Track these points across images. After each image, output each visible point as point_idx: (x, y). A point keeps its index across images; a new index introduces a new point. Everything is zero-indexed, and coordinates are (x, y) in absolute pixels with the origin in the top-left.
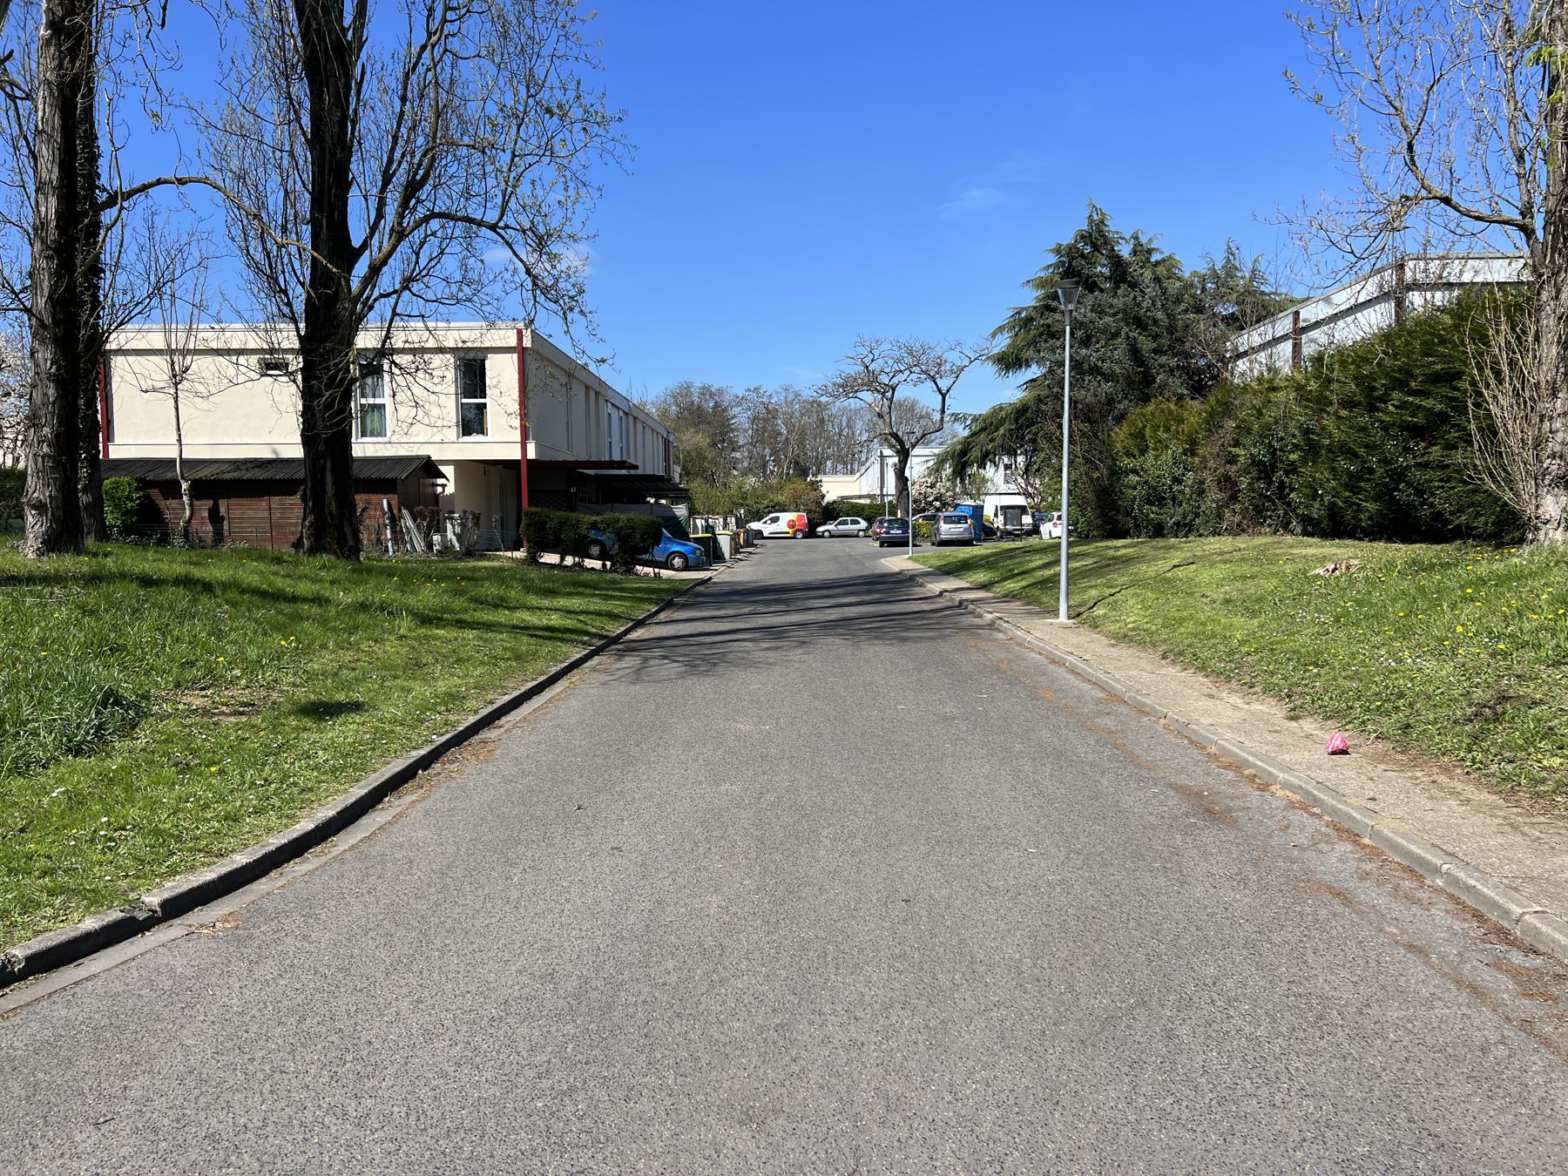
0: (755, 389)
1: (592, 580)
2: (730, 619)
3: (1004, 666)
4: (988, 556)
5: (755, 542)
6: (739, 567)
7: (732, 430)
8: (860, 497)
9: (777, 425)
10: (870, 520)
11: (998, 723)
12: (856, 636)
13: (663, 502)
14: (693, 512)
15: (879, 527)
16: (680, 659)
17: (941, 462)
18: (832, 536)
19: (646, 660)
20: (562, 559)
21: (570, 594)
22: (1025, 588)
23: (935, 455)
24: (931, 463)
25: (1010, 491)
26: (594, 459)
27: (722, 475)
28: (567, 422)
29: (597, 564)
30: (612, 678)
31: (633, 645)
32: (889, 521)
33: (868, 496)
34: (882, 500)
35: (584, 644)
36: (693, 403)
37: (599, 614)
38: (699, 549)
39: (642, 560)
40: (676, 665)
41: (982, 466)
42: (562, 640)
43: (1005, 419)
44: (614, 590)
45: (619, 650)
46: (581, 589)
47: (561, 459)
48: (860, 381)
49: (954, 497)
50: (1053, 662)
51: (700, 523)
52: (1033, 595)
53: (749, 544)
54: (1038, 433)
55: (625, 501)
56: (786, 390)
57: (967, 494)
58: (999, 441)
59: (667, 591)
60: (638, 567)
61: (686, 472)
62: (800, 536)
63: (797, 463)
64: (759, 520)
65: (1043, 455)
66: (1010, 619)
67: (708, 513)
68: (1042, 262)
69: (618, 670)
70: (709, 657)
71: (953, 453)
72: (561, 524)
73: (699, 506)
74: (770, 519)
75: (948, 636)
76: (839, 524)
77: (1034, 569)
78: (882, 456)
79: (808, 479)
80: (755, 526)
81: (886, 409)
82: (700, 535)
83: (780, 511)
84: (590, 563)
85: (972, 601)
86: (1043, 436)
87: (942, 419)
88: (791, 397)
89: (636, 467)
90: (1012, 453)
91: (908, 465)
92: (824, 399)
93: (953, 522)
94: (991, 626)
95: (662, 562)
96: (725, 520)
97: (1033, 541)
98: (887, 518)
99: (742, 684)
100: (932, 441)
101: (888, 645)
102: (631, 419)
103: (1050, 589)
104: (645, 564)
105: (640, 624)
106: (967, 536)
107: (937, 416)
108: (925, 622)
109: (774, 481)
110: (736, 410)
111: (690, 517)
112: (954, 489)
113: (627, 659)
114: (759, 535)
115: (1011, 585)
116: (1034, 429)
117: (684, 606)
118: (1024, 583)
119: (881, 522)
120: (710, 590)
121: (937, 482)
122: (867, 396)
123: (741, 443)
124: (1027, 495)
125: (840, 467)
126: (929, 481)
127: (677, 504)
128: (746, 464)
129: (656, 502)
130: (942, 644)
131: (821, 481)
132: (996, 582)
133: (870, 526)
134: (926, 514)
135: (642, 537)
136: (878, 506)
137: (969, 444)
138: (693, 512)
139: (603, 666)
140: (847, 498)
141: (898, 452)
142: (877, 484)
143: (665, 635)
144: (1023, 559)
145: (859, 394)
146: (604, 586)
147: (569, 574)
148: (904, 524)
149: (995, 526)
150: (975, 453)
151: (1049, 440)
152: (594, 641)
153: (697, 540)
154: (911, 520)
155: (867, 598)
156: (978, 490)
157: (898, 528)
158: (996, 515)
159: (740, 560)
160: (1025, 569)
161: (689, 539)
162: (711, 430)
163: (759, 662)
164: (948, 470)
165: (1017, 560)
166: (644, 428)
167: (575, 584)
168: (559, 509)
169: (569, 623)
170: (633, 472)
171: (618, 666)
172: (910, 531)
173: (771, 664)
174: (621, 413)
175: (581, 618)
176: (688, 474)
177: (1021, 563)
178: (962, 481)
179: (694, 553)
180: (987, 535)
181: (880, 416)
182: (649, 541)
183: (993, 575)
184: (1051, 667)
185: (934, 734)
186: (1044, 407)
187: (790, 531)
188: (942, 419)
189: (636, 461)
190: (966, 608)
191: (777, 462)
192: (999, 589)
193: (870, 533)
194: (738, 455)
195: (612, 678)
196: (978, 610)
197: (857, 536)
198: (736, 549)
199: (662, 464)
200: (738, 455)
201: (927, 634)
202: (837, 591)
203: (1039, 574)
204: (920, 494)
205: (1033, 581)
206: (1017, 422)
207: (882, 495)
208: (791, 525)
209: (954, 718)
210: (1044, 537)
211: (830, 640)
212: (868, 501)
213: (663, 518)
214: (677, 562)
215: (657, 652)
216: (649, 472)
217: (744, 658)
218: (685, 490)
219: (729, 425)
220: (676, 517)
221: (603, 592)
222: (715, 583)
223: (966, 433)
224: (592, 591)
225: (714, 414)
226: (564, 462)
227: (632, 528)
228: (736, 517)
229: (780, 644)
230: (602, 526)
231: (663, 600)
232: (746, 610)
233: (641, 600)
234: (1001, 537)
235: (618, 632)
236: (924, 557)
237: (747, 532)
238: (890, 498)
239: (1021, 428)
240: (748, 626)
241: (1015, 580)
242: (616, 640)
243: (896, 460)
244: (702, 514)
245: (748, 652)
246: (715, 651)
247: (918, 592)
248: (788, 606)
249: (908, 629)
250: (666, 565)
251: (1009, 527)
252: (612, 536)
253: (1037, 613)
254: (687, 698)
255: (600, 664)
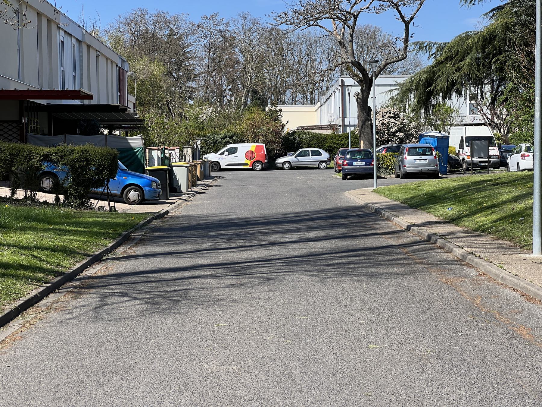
0: (212, 16)
1: (45, 214)
2: (190, 255)
3: (477, 302)
4: (456, 189)
5: (212, 174)
6: (197, 200)
7: (188, 59)
8: (321, 127)
9: (234, 53)
10: (331, 151)
11: (475, 363)
12: (323, 272)
13: (117, 133)
14: (148, 143)
15: (341, 159)
16: (140, 296)
17: (405, 92)
18: (292, 168)
19: (104, 297)
20: (13, 193)
21: (22, 229)
22: (495, 221)
23: (399, 85)
24: (396, 93)
25: (475, 122)
26: (46, 88)
27: (177, 105)
28: (19, 50)
29: (50, 198)
30: (70, 316)
31: (90, 281)
32: (353, 153)
33: (329, 127)
34: (344, 130)
35: (39, 281)
36: (147, 31)
37: (54, 249)
38: (156, 182)
39: (97, 193)
40: (136, 302)
41: (447, 95)
42: (16, 277)
43: (472, 47)
44: (68, 224)
45: (76, 287)
46: (34, 224)
47: (13, 89)
48: (321, 8)
49: (418, 127)
50: (528, 298)
51: (156, 154)
52: (503, 230)
53: (206, 176)
54: (505, 62)
55: (78, 131)
56: (244, 17)
57: (431, 125)
58: (465, 70)
59: (123, 225)
60: (93, 201)
61: (140, 103)
62: (259, 167)
63: (255, 92)
64: (216, 152)
65: (510, 85)
66: (481, 254)
67: (164, 143)
68: (459, 35)
69: (76, 307)
70: (169, 295)
71: (418, 83)
72: (13, 156)
73: (154, 136)
74: (227, 150)
75: (418, 271)
76: (299, 155)
77: (504, 203)
78: (343, 86)
79: (267, 109)
80: (211, 157)
81: (347, 37)
82: (156, 167)
83: (238, 142)
84: (41, 196)
85: (442, 236)
86: (512, 65)
87: (406, 48)
88: (249, 24)
89: (90, 97)
90: (479, 83)
91: (371, 94)
92: (283, 27)
93: (418, 154)
94: (462, 261)
95: (116, 196)
96: (181, 151)
97: (500, 173)
98: (350, 149)
99: (206, 322)
100: (394, 71)
101: (356, 281)
102: (84, 47)
103: (522, 223)
104: (101, 197)
105: (96, 259)
106: (432, 168)
107: (400, 45)
108: (393, 257)
109: (232, 111)
110: (192, 38)
111: (145, 148)
112: (418, 120)
113: (85, 296)
114: (216, 166)
115: (481, 219)
116: (501, 58)
117: (141, 241)
118: (494, 217)
119: (344, 153)
120: (165, 225)
121: (400, 112)
122: (329, 24)
123: (197, 72)
124: (493, 125)
125: (299, 97)
126: (392, 111)
127: (132, 135)
128: (202, 93)
129: (110, 133)
130: (412, 280)
131: (280, 111)
132: (466, 216)
133: (332, 158)
134: (390, 145)
135: (97, 169)
136: (340, 136)
137: (434, 74)
138: (148, 143)
139: (59, 305)
140: (308, 128)
141: (360, 82)
142: (339, 113)
143: (123, 271)
144: (491, 192)
145: (319, 22)
146: (58, 220)
147: (20, 208)
148: (367, 156)
149: (461, 157)
150: (441, 83)
151: (517, 67)
152: (50, 277)
153: (153, 172)
154: (375, 150)
155: (332, 232)
156: (443, 120)
157: (361, 160)
158: (461, 147)
159: (197, 193)
160: (494, 202)
161: (144, 172)
162: (167, 59)
163: (223, 300)
164: (412, 100)
165: (485, 193)
166: (98, 56)
167: (28, 218)
168: (10, 141)
169: (24, 259)
170: (86, 102)
171: (76, 303)
172: (374, 163)
173: (235, 301)
174: (74, 41)
175: (35, 254)
176: (142, 104)
177: (490, 196)
178: (427, 111)
179: (150, 186)
180: (452, 166)
181: (341, 44)
182: (105, 173)
183: (461, 209)
184: (527, 304)
185: (409, 374)
186: (511, 36)
187: (249, 162)
188: (406, 48)
189: (89, 90)
190: (435, 242)
191: (235, 92)
192: (469, 223)
193: (332, 164)
194: (193, 84)
195: (70, 316)
196: (448, 244)
197: (318, 168)
198: (193, 182)
199: (116, 94)
200: (193, 84)
201: (396, 270)
202: (301, 225)
203: (509, 208)
204: (383, 124)
205: (504, 214)
206: (483, 50)
207: (344, 126)
208: (249, 156)
209: (429, 358)
210: (511, 169)
211: (295, 276)
212: (329, 132)
213: (119, 149)
214: (133, 195)
215: (116, 289)
216: (103, 102)
217: (206, 296)
218: (140, 120)
219: (184, 54)
220: (132, 149)
221: (57, 227)
222: (172, 218)
223: (432, 62)
224: (46, 226)
225: (169, 42)
226: (15, 91)
227: (87, 160)
228: (193, 148)
229: (244, 281)
230: (55, 158)
231: (120, 235)
232: (206, 245)
233: (97, 235)
234: (468, 169)
235: (75, 268)
236: (389, 190)
237: (204, 163)
238: (353, 129)
239: (487, 56)
240: (209, 262)
241: (485, 213)
242: (72, 277)
243: (358, 89)
244: (158, 145)
245: (210, 289)
246: (176, 288)
247: (384, 226)
248: (250, 241)
249: (378, 264)
250: (121, 198)
251: (476, 159)
252: (66, 168)
253: (510, 248)
254: (149, 336)
255: (56, 302)
